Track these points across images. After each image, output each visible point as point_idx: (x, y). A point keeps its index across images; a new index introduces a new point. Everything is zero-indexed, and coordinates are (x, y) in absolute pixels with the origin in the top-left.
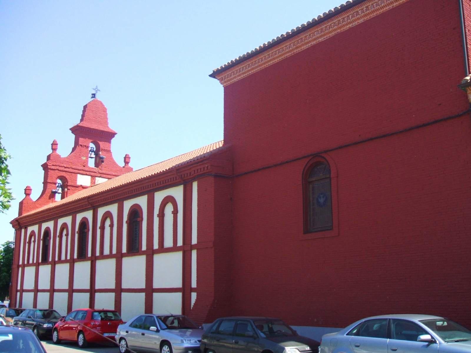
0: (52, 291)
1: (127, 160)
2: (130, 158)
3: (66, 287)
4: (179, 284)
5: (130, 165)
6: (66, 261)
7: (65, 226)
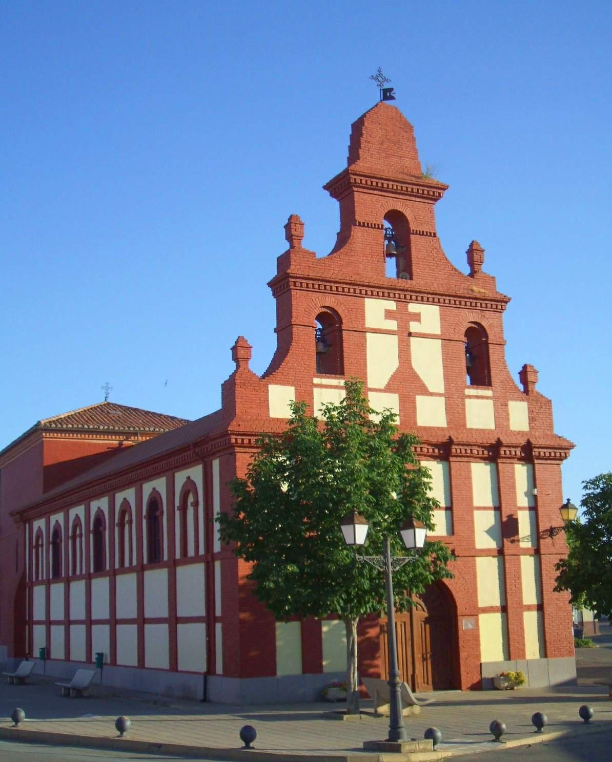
0: (114, 622)
1: (473, 254)
2: (482, 251)
3: (165, 614)
4: (202, 612)
5: (486, 268)
6: (196, 559)
7: (190, 486)
